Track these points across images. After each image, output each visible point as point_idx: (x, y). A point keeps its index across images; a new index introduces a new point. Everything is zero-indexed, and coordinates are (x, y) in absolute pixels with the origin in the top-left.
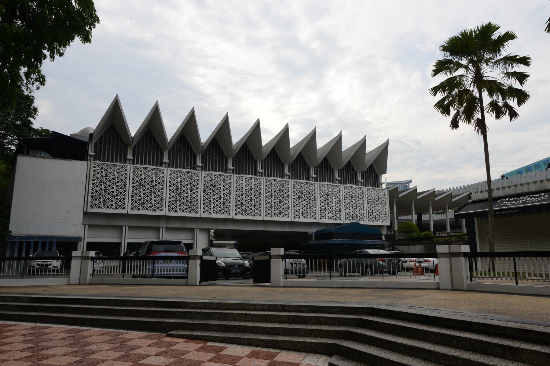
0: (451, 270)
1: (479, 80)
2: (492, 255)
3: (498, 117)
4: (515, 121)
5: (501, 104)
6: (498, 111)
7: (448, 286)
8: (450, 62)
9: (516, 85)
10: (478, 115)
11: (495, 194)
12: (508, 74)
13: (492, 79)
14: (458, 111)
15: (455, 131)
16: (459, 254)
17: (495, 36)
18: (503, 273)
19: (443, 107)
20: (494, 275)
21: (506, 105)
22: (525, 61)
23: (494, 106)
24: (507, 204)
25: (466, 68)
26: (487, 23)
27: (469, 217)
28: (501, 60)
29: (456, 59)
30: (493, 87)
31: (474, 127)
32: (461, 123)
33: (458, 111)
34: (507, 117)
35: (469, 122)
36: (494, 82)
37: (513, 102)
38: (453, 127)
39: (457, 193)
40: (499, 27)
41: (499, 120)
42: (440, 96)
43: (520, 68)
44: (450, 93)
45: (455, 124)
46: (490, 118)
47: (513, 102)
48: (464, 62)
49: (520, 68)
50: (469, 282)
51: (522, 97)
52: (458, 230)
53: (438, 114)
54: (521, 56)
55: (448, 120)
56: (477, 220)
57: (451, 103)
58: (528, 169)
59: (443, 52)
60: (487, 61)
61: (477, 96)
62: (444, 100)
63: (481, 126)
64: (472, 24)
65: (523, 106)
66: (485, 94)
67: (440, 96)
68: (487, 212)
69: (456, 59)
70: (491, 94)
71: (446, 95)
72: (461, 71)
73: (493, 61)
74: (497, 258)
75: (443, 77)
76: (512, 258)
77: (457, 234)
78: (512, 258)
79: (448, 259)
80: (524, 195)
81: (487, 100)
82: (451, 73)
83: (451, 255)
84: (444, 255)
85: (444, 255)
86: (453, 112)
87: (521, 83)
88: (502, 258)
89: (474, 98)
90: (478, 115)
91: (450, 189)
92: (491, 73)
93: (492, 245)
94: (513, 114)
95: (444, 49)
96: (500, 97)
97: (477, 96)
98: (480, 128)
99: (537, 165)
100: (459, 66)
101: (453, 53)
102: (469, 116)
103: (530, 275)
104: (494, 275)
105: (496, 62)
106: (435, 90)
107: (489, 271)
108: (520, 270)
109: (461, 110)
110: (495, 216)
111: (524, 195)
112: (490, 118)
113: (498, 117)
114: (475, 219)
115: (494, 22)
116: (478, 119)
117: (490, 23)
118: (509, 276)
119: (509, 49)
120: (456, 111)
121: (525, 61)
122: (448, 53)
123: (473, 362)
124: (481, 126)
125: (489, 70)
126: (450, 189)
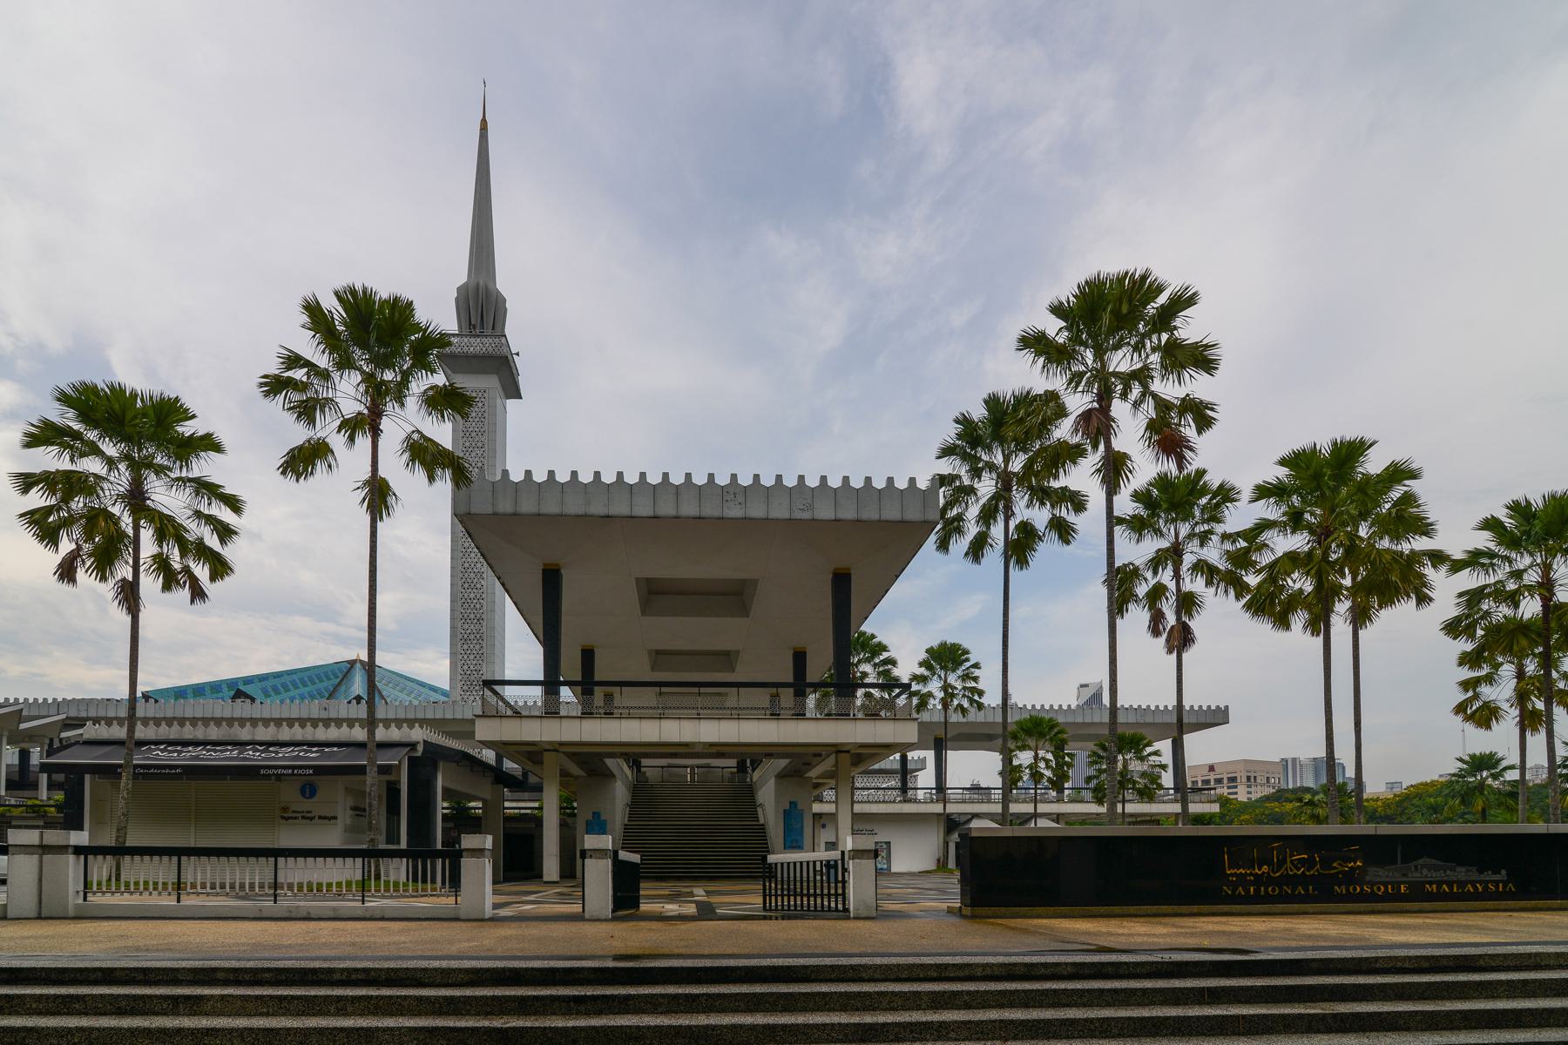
0: (40, 880)
1: (136, 499)
2: (119, 851)
3: (167, 587)
4: (199, 605)
5: (177, 566)
6: (170, 580)
7: (30, 907)
8: (77, 436)
9: (212, 541)
10: (124, 571)
11: (141, 732)
12: (198, 514)
13: (166, 512)
14: (79, 548)
15: (65, 587)
16: (62, 849)
17: (186, 429)
18: (156, 884)
19: (44, 527)
20: (118, 887)
21: (187, 570)
22: (234, 504)
23: (162, 563)
24: (161, 756)
25: (111, 463)
26: (173, 396)
27: (78, 771)
28: (190, 480)
29: (92, 435)
30: (167, 528)
31: (112, 594)
32: (81, 574)
33: (79, 548)
34: (185, 593)
35: (103, 579)
36: (170, 519)
37: (202, 572)
38: (61, 578)
39: (34, 712)
40: (194, 416)
41: (167, 595)
42: (37, 499)
43: (225, 515)
44: (66, 499)
45: (67, 572)
46: (150, 585)
47: (202, 572)
48: (110, 449)
49: (225, 515)
50: (81, 901)
51: (220, 568)
52: (27, 793)
53: (27, 540)
54: (228, 491)
55: (50, 559)
56: (92, 781)
57: (67, 523)
58: (198, 690)
59: (57, 405)
60: (160, 470)
61: (130, 532)
62: (48, 511)
63: (129, 595)
64: (136, 376)
65: (219, 584)
66: (147, 535)
67: (37, 499)
68: (120, 766)
69: (92, 435)
70: (161, 537)
71: (53, 502)
72: (92, 465)
73: (173, 475)
74: (127, 858)
75: (50, 459)
76: (175, 859)
77: (30, 803)
78: (175, 859)
79: (36, 857)
80: (196, 743)
81: (148, 547)
82: (72, 460)
83: (44, 849)
84: (26, 849)
85: (26, 849)
86: (66, 546)
87: (223, 541)
88: (156, 858)
89: (124, 535)
90: (124, 571)
91: (16, 700)
92: (167, 498)
93: (122, 830)
94: (198, 594)
95: (64, 399)
96: (176, 551)
97: (130, 532)
98: (126, 599)
99: (215, 687)
100: (95, 451)
101: (85, 416)
102: (103, 566)
103: (203, 886)
104: (118, 887)
105: (178, 479)
106: (26, 482)
107: (109, 880)
108: (188, 877)
109: (87, 547)
110: (135, 776)
111: (196, 743)
112: (150, 585)
113: (167, 587)
114: (87, 777)
115: (188, 402)
116: (124, 580)
117: (177, 399)
118: (146, 889)
119: (204, 466)
120: (73, 546)
121: (234, 504)
122: (71, 413)
123: (121, 1029)
124: (129, 595)
125: (162, 490)
126: (16, 700)
